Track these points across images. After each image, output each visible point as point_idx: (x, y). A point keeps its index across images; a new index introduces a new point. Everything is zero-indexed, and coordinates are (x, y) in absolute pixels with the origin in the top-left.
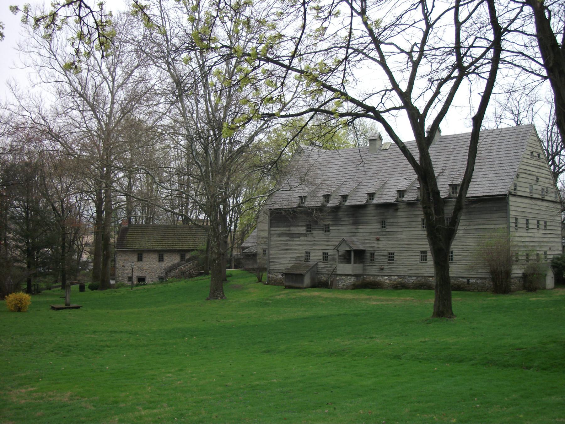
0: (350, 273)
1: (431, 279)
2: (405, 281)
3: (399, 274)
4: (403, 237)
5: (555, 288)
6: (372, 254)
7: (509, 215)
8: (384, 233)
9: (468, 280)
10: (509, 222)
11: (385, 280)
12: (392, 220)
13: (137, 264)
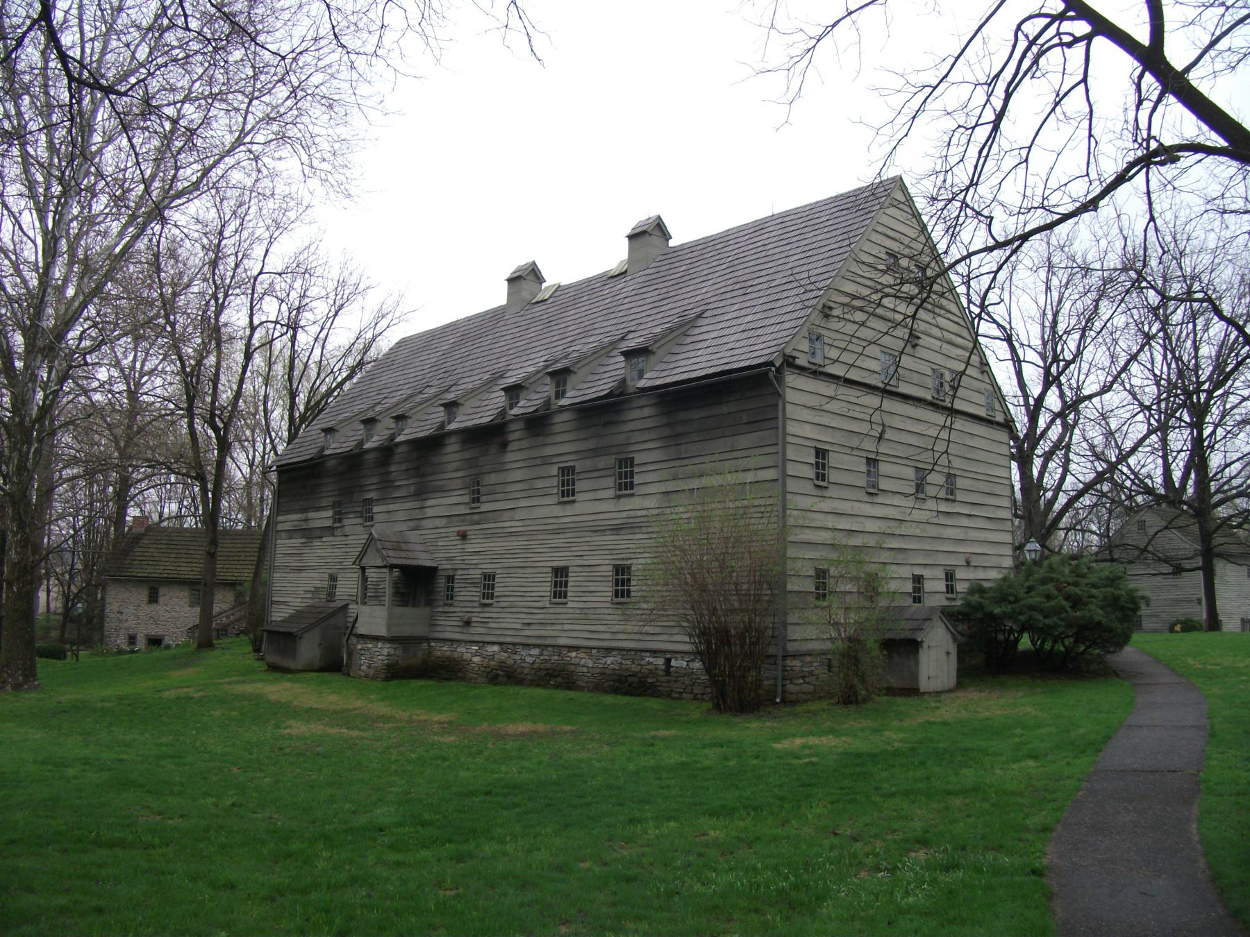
0: (382, 631)
1: (574, 654)
2: (515, 661)
3: (502, 639)
4: (516, 526)
5: (959, 686)
6: (451, 579)
7: (785, 433)
8: (476, 517)
9: (668, 661)
10: (785, 460)
11: (472, 656)
12: (493, 478)
13: (147, 609)
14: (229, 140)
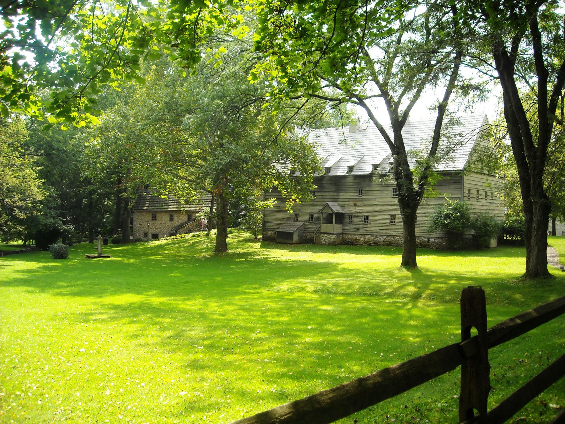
1: (398, 238)
4: (376, 203)
6: (351, 217)
8: (361, 199)
9: (429, 239)
12: (367, 189)
14: (305, 102)
